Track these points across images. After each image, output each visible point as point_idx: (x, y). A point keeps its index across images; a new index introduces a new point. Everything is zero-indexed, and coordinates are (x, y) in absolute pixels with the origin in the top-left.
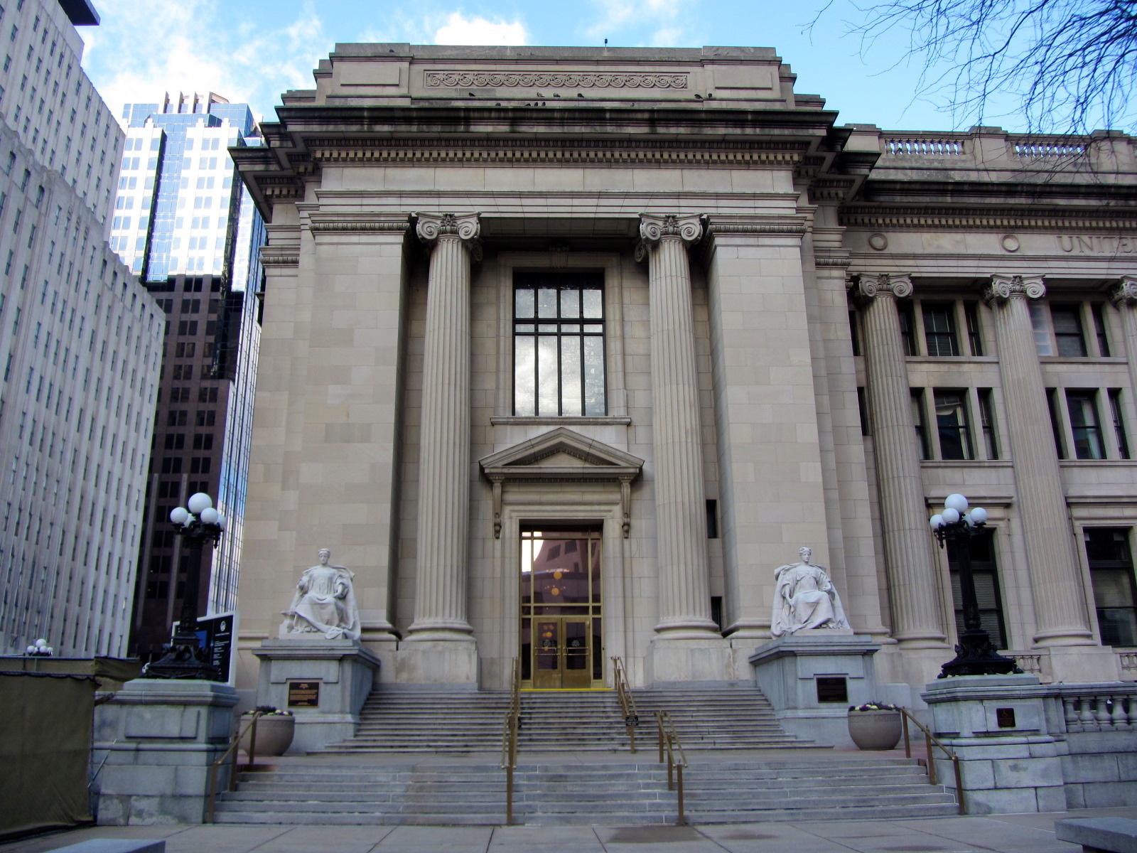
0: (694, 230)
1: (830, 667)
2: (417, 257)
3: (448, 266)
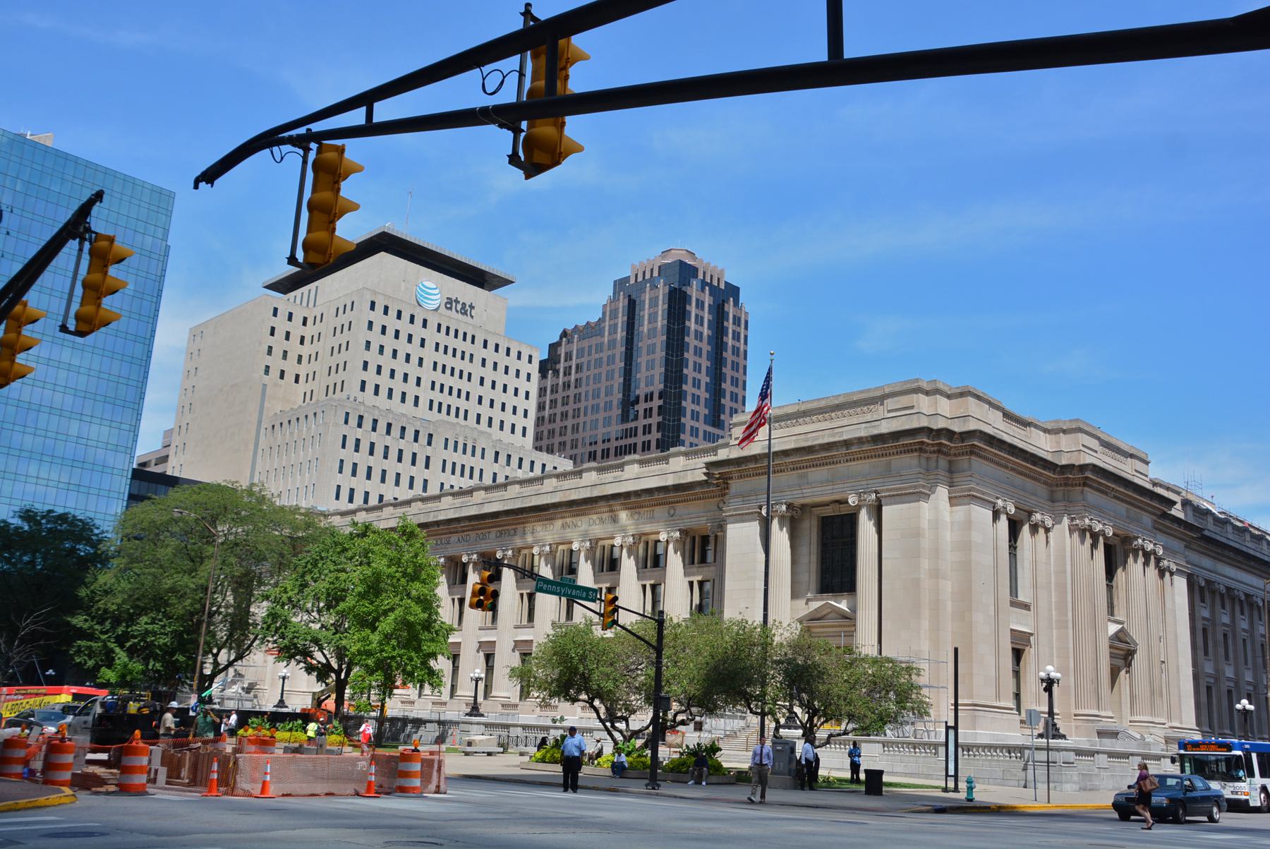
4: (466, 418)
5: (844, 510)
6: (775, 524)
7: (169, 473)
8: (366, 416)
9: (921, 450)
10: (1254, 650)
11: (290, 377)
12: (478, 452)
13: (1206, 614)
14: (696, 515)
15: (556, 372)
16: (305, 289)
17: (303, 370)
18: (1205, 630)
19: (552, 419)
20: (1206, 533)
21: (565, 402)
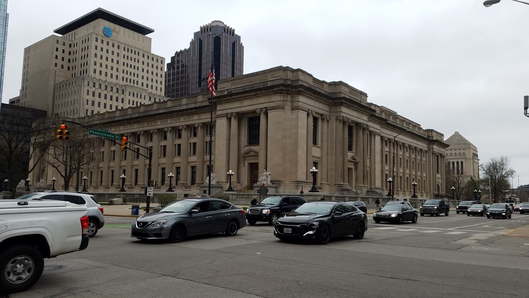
0: (264, 110)
1: (204, 189)
2: (229, 120)
3: (234, 123)
4: (137, 84)
5: (256, 115)
6: (233, 119)
7: (21, 105)
8: (96, 83)
9: (281, 93)
10: (404, 162)
11: (66, 68)
12: (143, 97)
13: (387, 150)
14: (206, 118)
15: (174, 68)
16: (70, 33)
17: (70, 65)
18: (386, 155)
19: (173, 85)
20: (389, 122)
21: (178, 79)
